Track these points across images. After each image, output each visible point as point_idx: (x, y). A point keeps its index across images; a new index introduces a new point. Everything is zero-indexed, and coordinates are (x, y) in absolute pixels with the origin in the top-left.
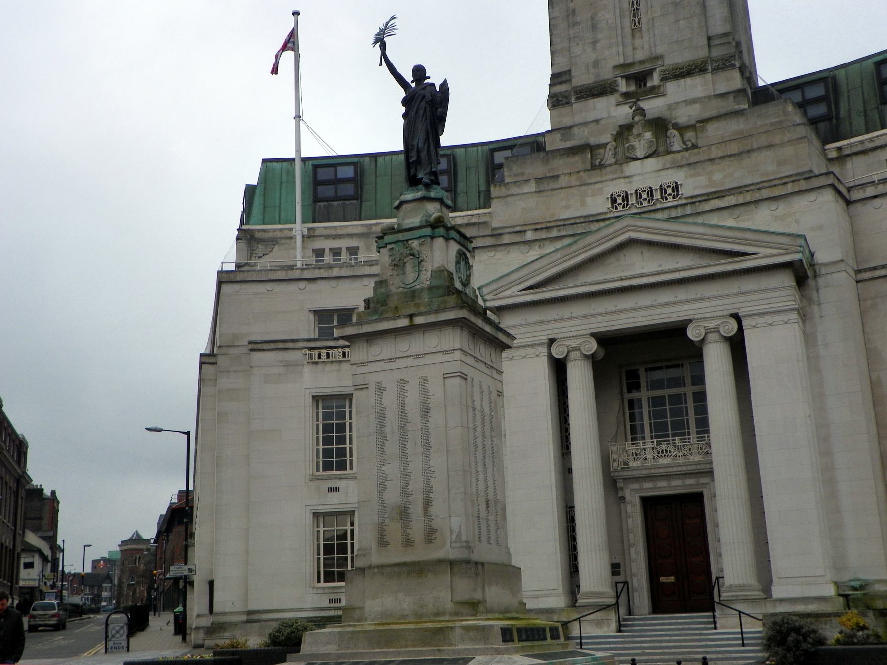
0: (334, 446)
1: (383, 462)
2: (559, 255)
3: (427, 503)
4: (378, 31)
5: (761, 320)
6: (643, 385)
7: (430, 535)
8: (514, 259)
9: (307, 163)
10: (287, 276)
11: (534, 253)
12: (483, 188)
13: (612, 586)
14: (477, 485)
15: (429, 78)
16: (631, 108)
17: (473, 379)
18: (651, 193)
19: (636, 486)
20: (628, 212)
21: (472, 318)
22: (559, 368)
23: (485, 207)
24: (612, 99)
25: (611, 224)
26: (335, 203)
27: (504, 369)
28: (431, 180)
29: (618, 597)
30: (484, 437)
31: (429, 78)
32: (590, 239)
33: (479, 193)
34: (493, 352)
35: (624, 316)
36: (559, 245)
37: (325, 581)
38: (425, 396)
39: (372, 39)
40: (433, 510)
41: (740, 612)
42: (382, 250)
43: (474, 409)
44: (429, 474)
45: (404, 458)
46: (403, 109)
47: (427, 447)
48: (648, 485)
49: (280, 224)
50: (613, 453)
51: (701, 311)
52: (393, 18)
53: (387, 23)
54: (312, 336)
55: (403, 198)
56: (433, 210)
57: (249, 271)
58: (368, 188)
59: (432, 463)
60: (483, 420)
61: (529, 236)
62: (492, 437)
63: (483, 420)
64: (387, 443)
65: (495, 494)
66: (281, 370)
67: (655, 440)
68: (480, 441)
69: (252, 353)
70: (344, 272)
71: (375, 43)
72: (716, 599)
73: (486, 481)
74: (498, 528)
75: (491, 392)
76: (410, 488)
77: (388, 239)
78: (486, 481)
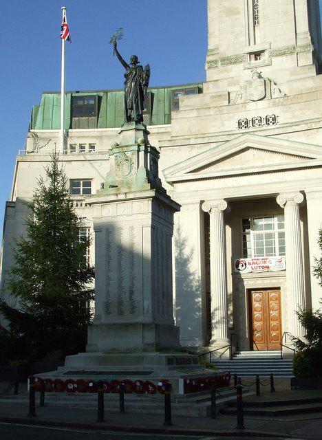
3: (132, 293)
7: (133, 309)
8: (184, 153)
11: (195, 152)
12: (167, 112)
18: (261, 120)
22: (205, 218)
36: (208, 147)
40: (134, 297)
44: (133, 278)
45: (120, 268)
61: (193, 141)
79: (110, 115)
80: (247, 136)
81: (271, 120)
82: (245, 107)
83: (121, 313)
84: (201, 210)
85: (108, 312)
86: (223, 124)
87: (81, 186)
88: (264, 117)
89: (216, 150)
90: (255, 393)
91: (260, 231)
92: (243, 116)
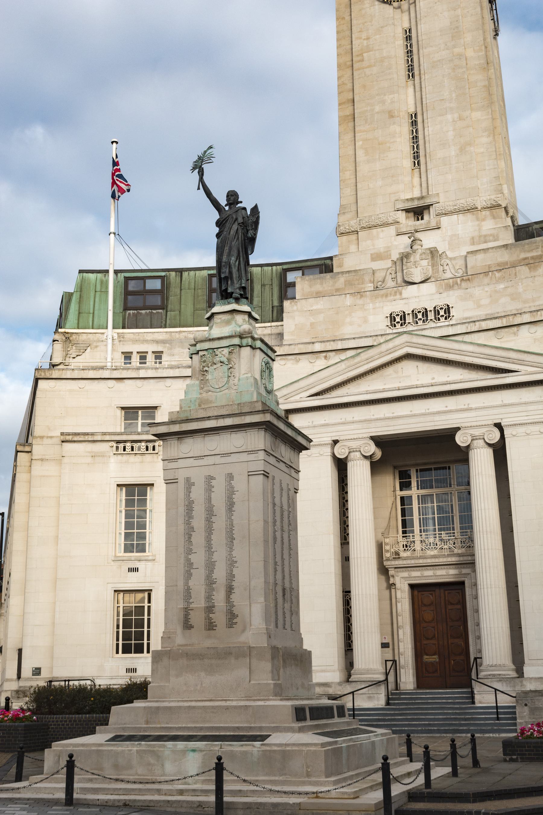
0: (135, 531)
1: (189, 551)
2: (343, 366)
3: (230, 590)
4: (196, 158)
5: (521, 430)
6: (414, 484)
8: (305, 366)
9: (119, 275)
10: (95, 377)
11: (321, 363)
12: (276, 303)
13: (382, 663)
14: (275, 575)
15: (241, 202)
16: (409, 238)
17: (274, 477)
19: (405, 574)
20: (405, 330)
21: (275, 422)
22: (341, 466)
23: (277, 321)
24: (392, 230)
25: (391, 339)
26: (143, 312)
27: (301, 469)
28: (241, 295)
29: (387, 674)
30: (282, 530)
31: (241, 202)
32: (372, 352)
33: (273, 307)
34: (292, 452)
35: (401, 421)
37: (123, 653)
38: (231, 492)
39: (191, 165)
41: (496, 690)
42: (194, 356)
43: (274, 505)
44: (232, 563)
46: (217, 230)
47: (231, 539)
48: (416, 573)
49: (93, 328)
50: (387, 544)
51: (470, 418)
52: (211, 147)
53: (205, 152)
54: (118, 430)
55: (215, 309)
56: (241, 323)
57: (63, 369)
58: (173, 299)
59: (234, 553)
60: (282, 515)
62: (289, 531)
63: (282, 515)
64: (193, 534)
65: (291, 583)
66: (89, 460)
67: (423, 534)
68: (278, 534)
69: (63, 444)
70: (150, 373)
71: (194, 169)
72: (474, 676)
73: (283, 571)
74: (292, 614)
75: (289, 490)
76: (214, 576)
77: (199, 347)
78: (283, 571)
79: (188, 308)
80: (404, 338)
81: (398, 319)
82: (401, 294)
83: (210, 626)
84: (334, 456)
85: (187, 625)
86: (365, 321)
87: (140, 418)
88: (408, 311)
89: (358, 359)
90: (449, 769)
91: (338, 445)
92: (397, 307)
